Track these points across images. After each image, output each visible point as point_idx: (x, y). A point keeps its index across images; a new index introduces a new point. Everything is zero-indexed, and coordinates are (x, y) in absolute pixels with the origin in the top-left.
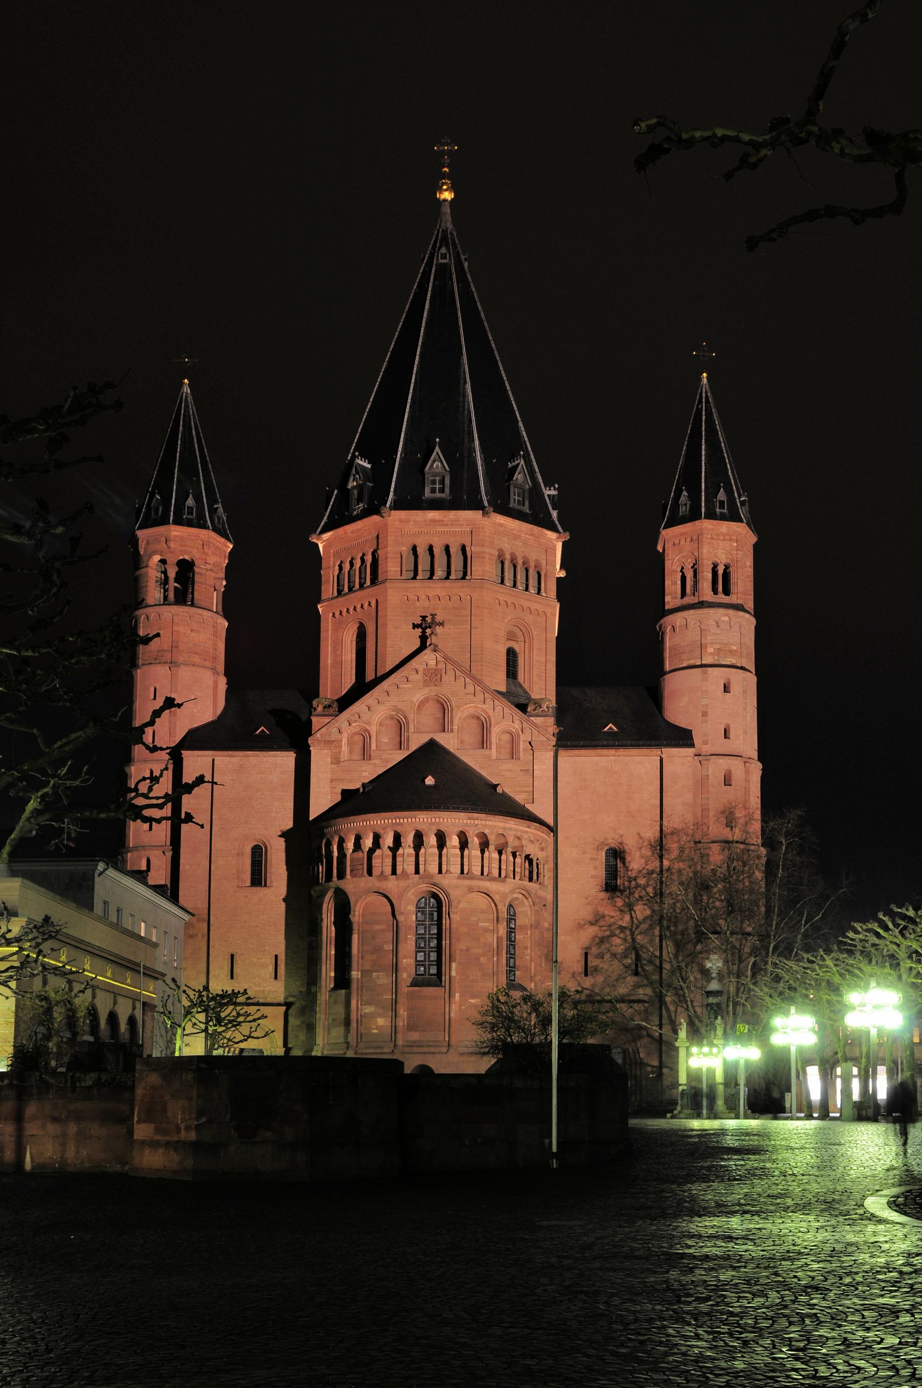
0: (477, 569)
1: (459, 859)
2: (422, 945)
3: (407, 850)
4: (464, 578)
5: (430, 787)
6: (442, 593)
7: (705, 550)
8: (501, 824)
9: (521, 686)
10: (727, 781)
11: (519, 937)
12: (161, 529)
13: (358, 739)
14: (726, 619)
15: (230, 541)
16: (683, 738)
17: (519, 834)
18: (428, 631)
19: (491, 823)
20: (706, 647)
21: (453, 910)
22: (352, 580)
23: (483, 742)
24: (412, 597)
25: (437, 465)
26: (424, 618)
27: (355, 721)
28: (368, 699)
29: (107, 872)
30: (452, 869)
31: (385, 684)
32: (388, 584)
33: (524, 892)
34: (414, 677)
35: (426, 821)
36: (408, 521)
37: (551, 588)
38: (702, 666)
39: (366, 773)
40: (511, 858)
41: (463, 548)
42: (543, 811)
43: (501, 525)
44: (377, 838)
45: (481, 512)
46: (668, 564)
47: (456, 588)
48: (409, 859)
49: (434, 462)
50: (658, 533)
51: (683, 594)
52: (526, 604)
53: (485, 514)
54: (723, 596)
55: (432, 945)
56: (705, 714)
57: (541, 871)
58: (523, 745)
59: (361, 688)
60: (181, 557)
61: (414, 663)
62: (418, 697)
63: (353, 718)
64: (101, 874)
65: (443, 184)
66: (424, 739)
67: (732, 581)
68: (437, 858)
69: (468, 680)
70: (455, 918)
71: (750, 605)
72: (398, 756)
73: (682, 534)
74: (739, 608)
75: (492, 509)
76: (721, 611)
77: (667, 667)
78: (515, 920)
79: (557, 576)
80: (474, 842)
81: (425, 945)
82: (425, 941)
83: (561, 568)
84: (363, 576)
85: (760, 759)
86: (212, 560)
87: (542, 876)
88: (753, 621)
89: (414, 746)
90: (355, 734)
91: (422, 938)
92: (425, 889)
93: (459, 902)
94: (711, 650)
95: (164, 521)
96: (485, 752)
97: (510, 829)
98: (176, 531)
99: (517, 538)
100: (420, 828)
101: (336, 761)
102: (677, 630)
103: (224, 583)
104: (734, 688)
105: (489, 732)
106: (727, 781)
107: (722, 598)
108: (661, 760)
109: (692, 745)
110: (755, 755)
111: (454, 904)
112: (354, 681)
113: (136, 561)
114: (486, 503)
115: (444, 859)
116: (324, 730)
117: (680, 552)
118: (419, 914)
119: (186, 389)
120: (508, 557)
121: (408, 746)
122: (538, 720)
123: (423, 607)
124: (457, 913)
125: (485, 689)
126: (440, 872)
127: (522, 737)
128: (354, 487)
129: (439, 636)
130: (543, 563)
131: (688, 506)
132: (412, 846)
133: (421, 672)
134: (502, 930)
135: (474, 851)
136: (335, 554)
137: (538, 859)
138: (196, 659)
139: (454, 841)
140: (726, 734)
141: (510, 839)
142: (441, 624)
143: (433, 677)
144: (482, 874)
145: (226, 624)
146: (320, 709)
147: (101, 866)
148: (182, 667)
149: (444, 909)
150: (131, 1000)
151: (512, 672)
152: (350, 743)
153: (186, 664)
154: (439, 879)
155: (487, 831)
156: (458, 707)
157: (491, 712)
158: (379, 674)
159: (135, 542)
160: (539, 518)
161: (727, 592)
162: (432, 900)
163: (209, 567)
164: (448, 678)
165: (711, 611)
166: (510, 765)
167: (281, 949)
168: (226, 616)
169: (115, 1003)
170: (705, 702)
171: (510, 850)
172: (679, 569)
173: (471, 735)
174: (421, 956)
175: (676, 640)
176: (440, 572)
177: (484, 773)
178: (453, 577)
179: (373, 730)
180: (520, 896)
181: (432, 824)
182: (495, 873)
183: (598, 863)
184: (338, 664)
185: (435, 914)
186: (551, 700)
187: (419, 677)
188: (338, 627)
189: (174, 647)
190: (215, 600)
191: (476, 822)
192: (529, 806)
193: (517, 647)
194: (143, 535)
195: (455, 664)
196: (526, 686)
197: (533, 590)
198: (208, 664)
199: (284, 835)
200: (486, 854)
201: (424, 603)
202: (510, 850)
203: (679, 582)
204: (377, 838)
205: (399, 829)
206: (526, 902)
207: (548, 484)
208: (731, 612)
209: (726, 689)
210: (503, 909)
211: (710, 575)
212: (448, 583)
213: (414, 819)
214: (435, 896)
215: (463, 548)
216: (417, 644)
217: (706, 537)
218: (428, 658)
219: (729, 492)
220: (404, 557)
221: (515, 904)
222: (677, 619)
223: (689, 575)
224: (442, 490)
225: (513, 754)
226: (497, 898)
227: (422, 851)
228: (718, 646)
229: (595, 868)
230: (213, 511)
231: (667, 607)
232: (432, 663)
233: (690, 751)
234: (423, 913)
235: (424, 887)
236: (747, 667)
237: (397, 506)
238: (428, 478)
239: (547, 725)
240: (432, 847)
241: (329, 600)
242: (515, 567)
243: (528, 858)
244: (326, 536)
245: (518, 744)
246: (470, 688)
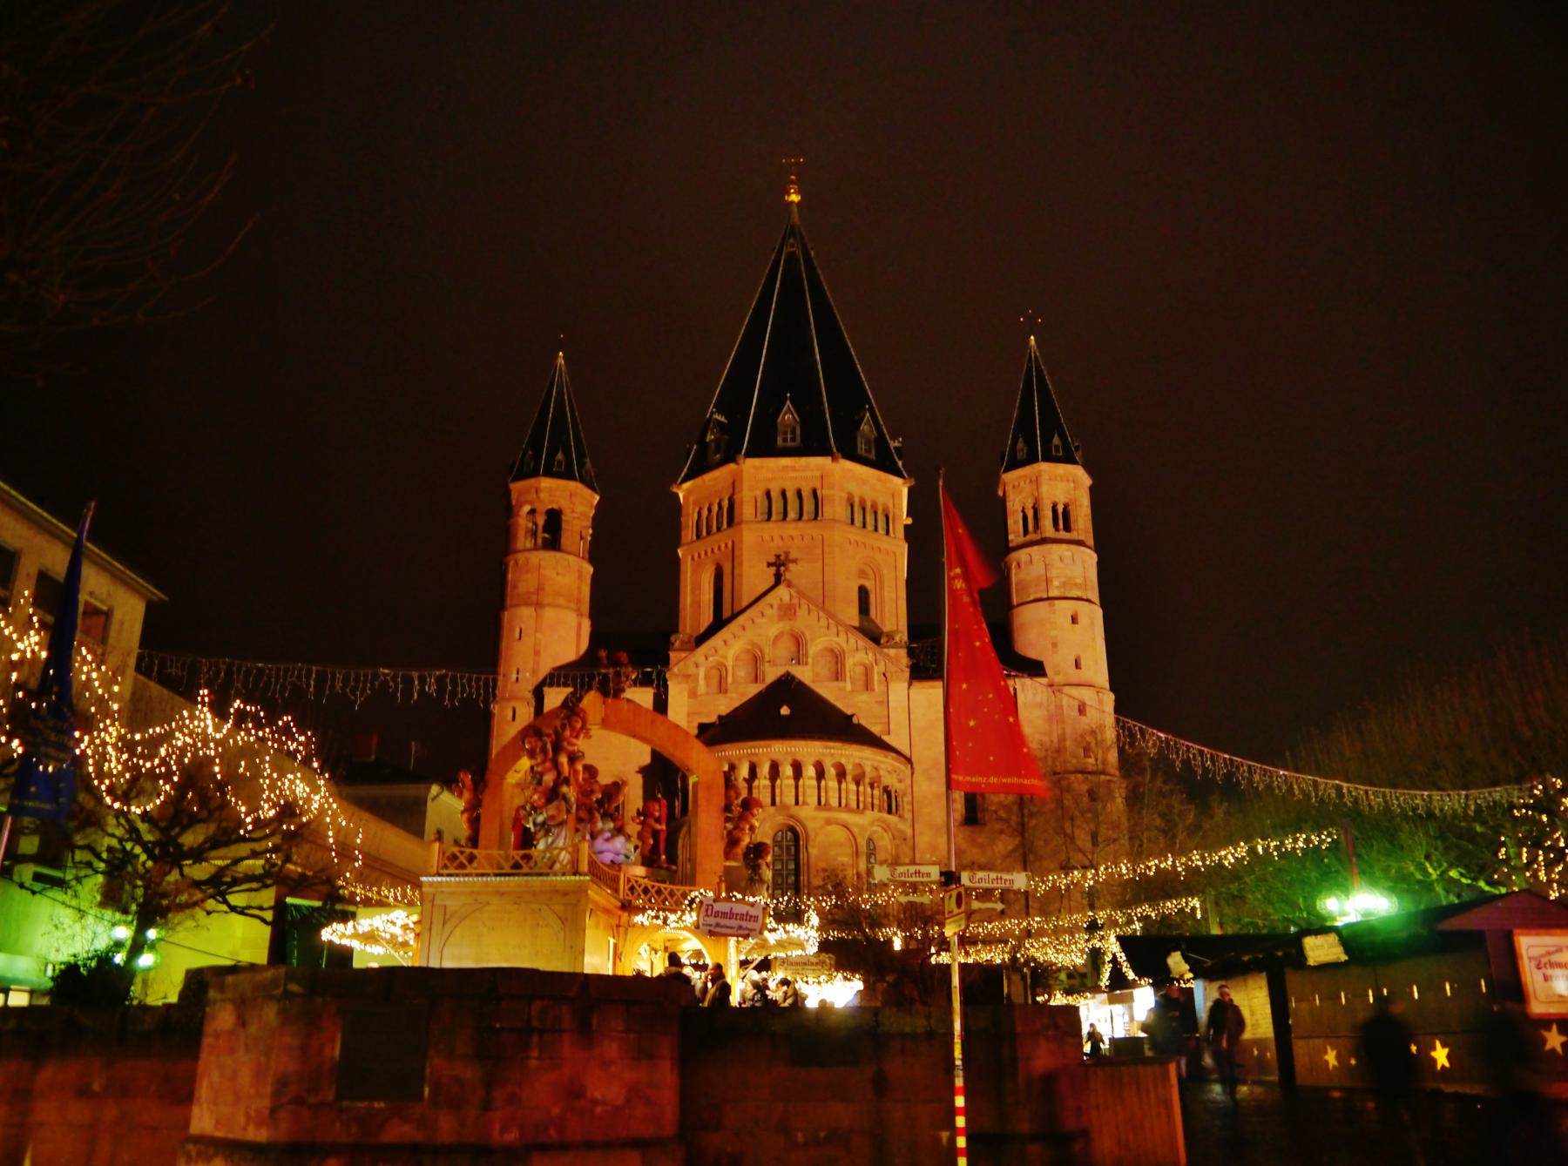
0: (828, 510)
1: (816, 791)
2: (780, 882)
3: (763, 782)
4: (816, 518)
5: (785, 716)
6: (795, 533)
7: (1044, 490)
8: (858, 753)
9: (872, 621)
10: (1082, 710)
12: (531, 482)
13: (715, 673)
14: (1069, 554)
15: (596, 492)
16: (1035, 669)
17: (876, 764)
18: (782, 569)
19: (847, 752)
20: (1052, 581)
21: (811, 843)
22: (710, 523)
23: (838, 675)
24: (767, 537)
25: (788, 416)
26: (778, 557)
27: (712, 656)
28: (724, 634)
29: (441, 796)
30: (808, 800)
31: (741, 619)
32: (744, 526)
33: (883, 825)
34: (768, 611)
35: (781, 750)
36: (761, 468)
37: (901, 532)
38: (1048, 599)
39: (724, 705)
40: (869, 790)
41: (814, 492)
43: (849, 470)
45: (830, 458)
46: (1009, 505)
47: (809, 529)
48: (765, 791)
49: (785, 414)
50: (999, 477)
51: (1026, 532)
52: (876, 544)
53: (834, 459)
54: (1064, 533)
55: (790, 881)
56: (1055, 645)
57: (900, 803)
58: (876, 677)
59: (719, 623)
60: (550, 507)
61: (769, 598)
62: (773, 631)
63: (710, 653)
64: (434, 798)
65: (791, 189)
66: (780, 671)
67: (1072, 518)
68: (793, 790)
69: (821, 614)
71: (1091, 542)
72: (753, 690)
73: (1021, 477)
74: (1080, 543)
75: (840, 455)
76: (1064, 546)
77: (1015, 602)
78: (875, 855)
79: (905, 523)
80: (831, 772)
81: (783, 882)
82: (783, 877)
83: (907, 516)
84: (720, 520)
85: (1112, 689)
86: (580, 509)
87: (901, 808)
88: (1095, 557)
90: (712, 668)
91: (779, 874)
92: (782, 821)
93: (817, 835)
94: (1056, 583)
95: (534, 474)
96: (840, 684)
97: (867, 759)
98: (546, 483)
99: (864, 482)
100: (775, 757)
101: (693, 694)
102: (1023, 566)
103: (591, 531)
104: (1082, 619)
105: (843, 664)
106: (1082, 710)
107: (1063, 535)
109: (1045, 675)
110: (1107, 685)
111: (812, 835)
112: (711, 619)
113: (509, 511)
114: (835, 450)
115: (800, 790)
116: (682, 664)
117: (1020, 492)
118: (776, 849)
119: (561, 361)
121: (763, 680)
122: (892, 652)
123: (777, 546)
124: (813, 847)
125: (839, 623)
126: (797, 803)
127: (876, 669)
128: (712, 441)
129: (793, 572)
130: (891, 506)
131: (1025, 451)
132: (768, 776)
133: (775, 607)
135: (831, 782)
136: (695, 503)
137: (896, 791)
138: (561, 601)
139: (809, 771)
140: (1078, 665)
141: (868, 769)
142: (795, 561)
143: (788, 611)
144: (840, 805)
145: (592, 570)
146: (677, 644)
147: (435, 789)
148: (547, 609)
149: (801, 843)
151: (864, 607)
152: (707, 677)
153: (549, 605)
154: (795, 810)
155: (843, 761)
156: (813, 640)
158: (737, 609)
159: (508, 493)
160: (884, 463)
161: (1067, 528)
162: (789, 834)
163: (576, 515)
164: (802, 613)
165: (1055, 547)
166: (865, 696)
168: (592, 561)
171: (867, 780)
172: (1020, 509)
173: (825, 670)
175: (1022, 575)
176: (792, 514)
177: (839, 705)
178: (805, 517)
179: (730, 664)
180: (880, 829)
181: (787, 753)
182: (853, 804)
184: (697, 604)
185: (793, 848)
186: (902, 636)
187: (775, 612)
188: (697, 568)
189: (540, 589)
190: (583, 547)
191: (832, 751)
192: (886, 738)
193: (869, 584)
194: (516, 487)
195: (811, 601)
196: (878, 621)
197: (882, 531)
199: (643, 771)
200: (844, 785)
201: (777, 543)
202: (867, 780)
203: (1021, 522)
205: (754, 759)
206: (885, 834)
207: (894, 438)
208: (1073, 547)
209: (1074, 620)
210: (862, 843)
211: (1050, 514)
212: (800, 524)
213: (769, 750)
214: (792, 830)
215: (814, 492)
216: (772, 581)
217: (1045, 477)
218: (782, 593)
219: (1063, 437)
220: (759, 500)
221: (875, 837)
222: (1022, 555)
223: (1030, 514)
224: (793, 440)
225: (868, 686)
226: (855, 830)
227: (778, 782)
228: (1063, 580)
230: (581, 465)
231: (1011, 545)
232: (786, 598)
233: (1044, 680)
234: (781, 847)
235: (780, 819)
236: (1093, 600)
237: (749, 455)
238: (780, 428)
239: (900, 656)
240: (788, 778)
241: (687, 544)
242: (864, 509)
243: (887, 791)
244: (686, 485)
245: (872, 674)
246: (824, 622)
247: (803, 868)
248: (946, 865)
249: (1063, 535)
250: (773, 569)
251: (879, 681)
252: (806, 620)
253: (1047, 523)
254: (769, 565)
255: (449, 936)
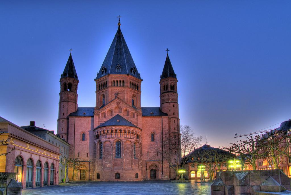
11: (136, 149)
23: (128, 115)
41: (259, 166)
42: (140, 126)
44: (108, 131)
51: (165, 90)
56: (170, 110)
66: (117, 114)
70: (123, 145)
89: (114, 115)
101: (99, 118)
108: (162, 118)
109: (168, 116)
120: (132, 83)
134: (133, 148)
140: (174, 114)
150: (39, 156)
157: (129, 110)
161: (173, 90)
167: (88, 152)
169: (31, 156)
170: (170, 108)
174: (117, 153)
179: (106, 112)
183: (150, 136)
185: (103, 151)
198: (74, 102)
204: (108, 131)
209: (174, 106)
210: (133, 144)
214: (120, 142)
216: (115, 98)
225: (134, 117)
229: (150, 137)
232: (118, 101)
234: (117, 145)
247: (122, 149)
248: (118, 176)
249: (172, 91)
250: (115, 95)
251: (136, 116)
252: (121, 105)
253: (169, 89)
254: (114, 95)
255: (74, 151)
